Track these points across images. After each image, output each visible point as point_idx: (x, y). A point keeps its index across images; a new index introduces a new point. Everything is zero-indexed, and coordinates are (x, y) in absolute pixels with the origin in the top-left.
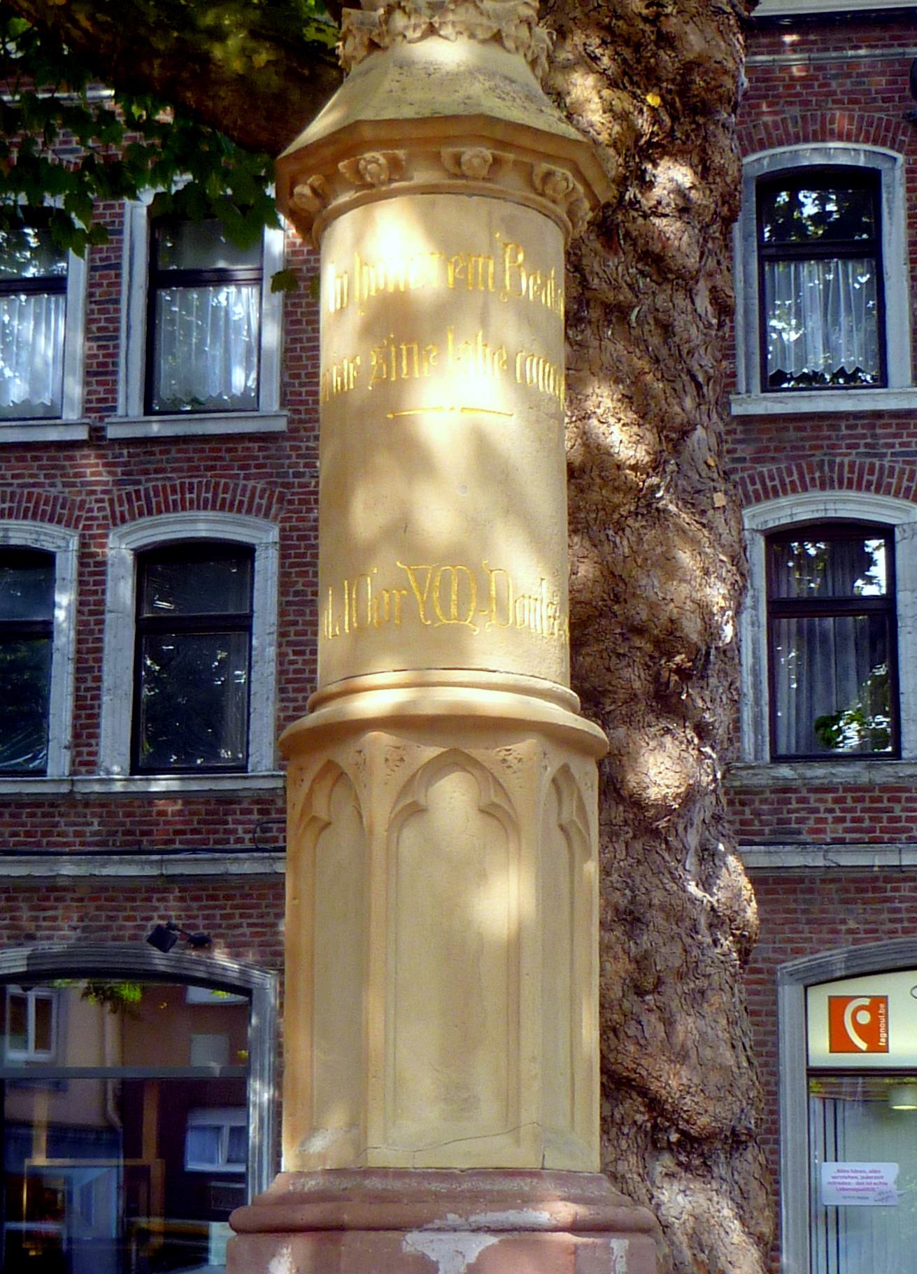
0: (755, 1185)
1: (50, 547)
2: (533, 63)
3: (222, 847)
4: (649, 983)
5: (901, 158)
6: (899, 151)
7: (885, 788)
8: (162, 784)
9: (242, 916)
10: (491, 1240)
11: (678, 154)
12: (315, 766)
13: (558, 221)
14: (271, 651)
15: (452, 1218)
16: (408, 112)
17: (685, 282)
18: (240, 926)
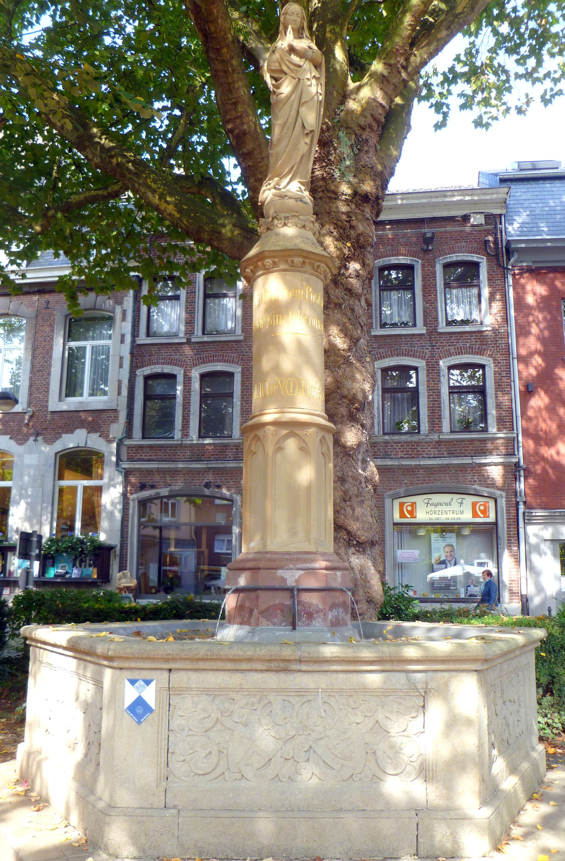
0: (378, 556)
1: (175, 373)
2: (314, 234)
3: (225, 460)
4: (347, 498)
5: (420, 261)
7: (415, 442)
8: (207, 441)
10: (302, 572)
11: (356, 260)
12: (251, 436)
13: (321, 279)
14: (239, 403)
15: (291, 566)
16: (278, 248)
17: (358, 297)
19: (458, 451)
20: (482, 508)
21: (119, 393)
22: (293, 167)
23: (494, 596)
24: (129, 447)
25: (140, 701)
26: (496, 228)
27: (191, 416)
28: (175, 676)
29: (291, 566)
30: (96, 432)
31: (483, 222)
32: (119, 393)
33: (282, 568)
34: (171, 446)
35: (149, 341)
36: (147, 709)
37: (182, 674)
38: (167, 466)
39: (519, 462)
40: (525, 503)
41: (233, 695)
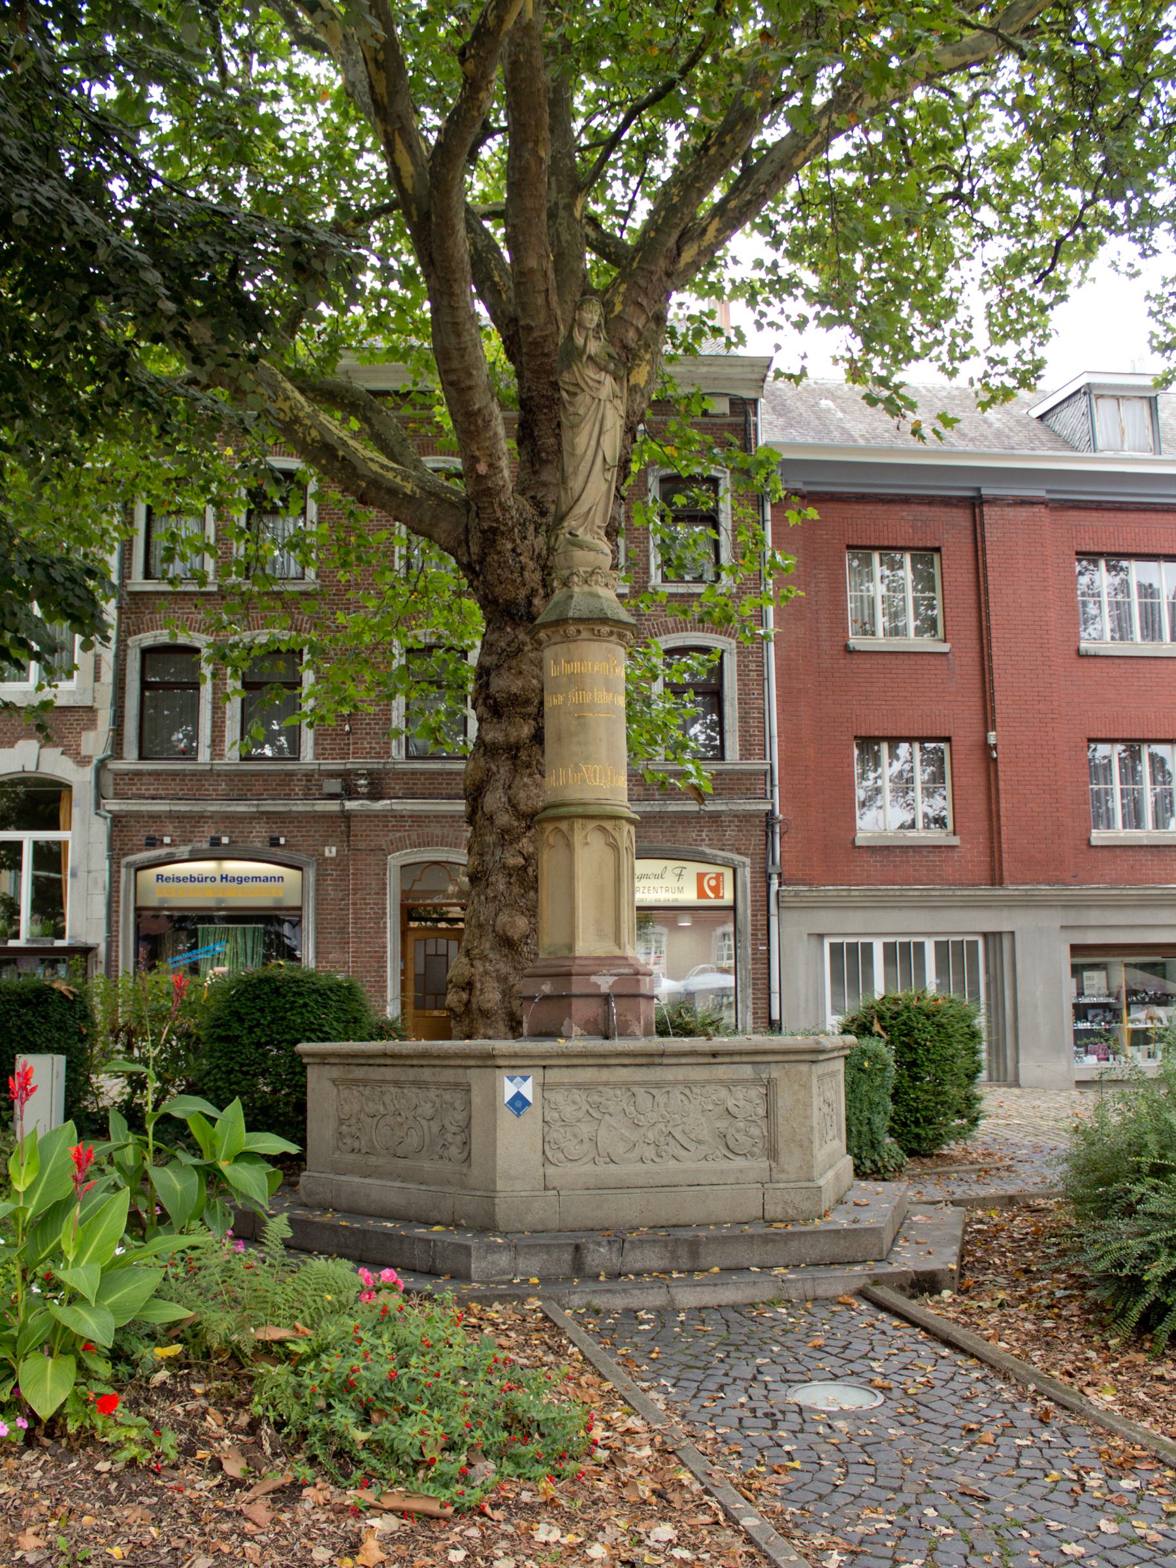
20: (713, 883)
21: (97, 678)
24: (119, 775)
25: (518, 1096)
26: (747, 421)
27: (228, 723)
28: (549, 1072)
30: (56, 746)
31: (727, 411)
32: (97, 678)
33: (594, 974)
34: (194, 774)
35: (150, 586)
36: (526, 1103)
37: (556, 1070)
38: (183, 808)
39: (772, 812)
40: (780, 875)
41: (601, 1088)
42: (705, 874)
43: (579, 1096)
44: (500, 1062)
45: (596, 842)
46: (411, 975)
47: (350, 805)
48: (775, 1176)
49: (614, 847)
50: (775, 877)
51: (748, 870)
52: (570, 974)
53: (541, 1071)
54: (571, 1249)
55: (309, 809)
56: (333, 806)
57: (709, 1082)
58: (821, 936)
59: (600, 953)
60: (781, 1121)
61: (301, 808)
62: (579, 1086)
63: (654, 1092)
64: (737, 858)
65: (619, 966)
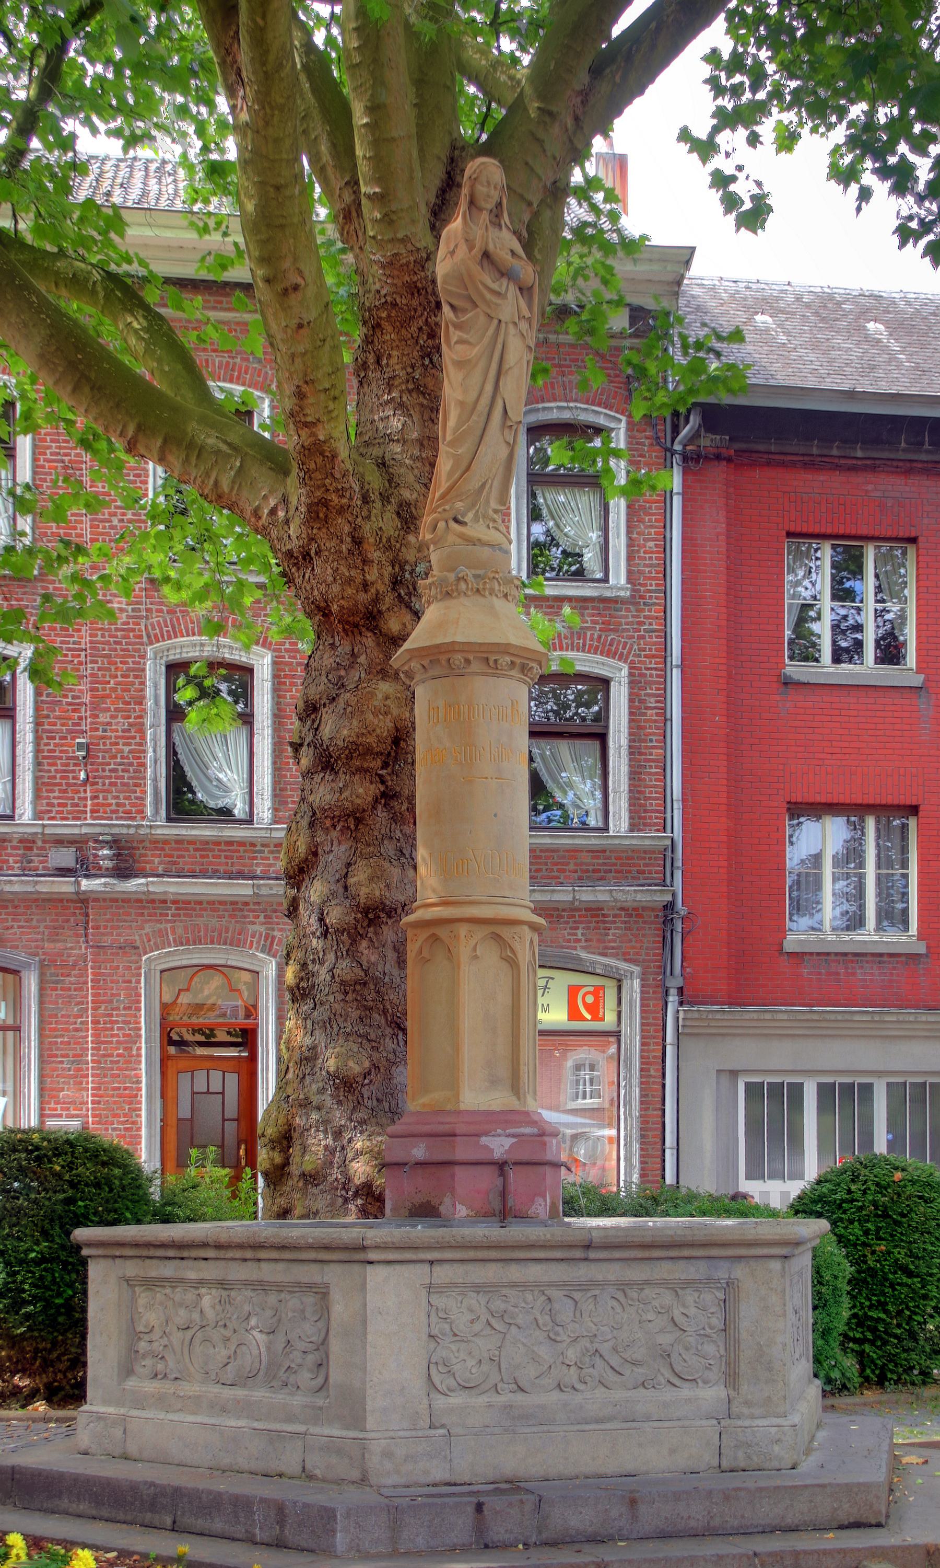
6: (622, 414)
9: (13, 920)
10: (514, 1140)
18: (12, 927)
19: (544, 873)
20: (590, 999)
22: (483, 485)
23: (421, 1205)
28: (437, 1269)
29: (499, 1131)
33: (486, 1134)
37: (446, 1267)
40: (681, 991)
41: (505, 1291)
42: (580, 987)
43: (473, 1300)
44: (372, 1256)
45: (490, 956)
46: (172, 1121)
47: (86, 884)
48: (735, 1410)
49: (512, 963)
50: (673, 992)
51: (637, 983)
52: (455, 1135)
53: (427, 1267)
54: (470, 1509)
55: (30, 889)
56: (64, 886)
57: (647, 1283)
58: (734, 1074)
59: (496, 1106)
60: (744, 1335)
61: (17, 888)
62: (478, 1288)
63: (577, 1295)
64: (623, 965)
65: (518, 1124)
